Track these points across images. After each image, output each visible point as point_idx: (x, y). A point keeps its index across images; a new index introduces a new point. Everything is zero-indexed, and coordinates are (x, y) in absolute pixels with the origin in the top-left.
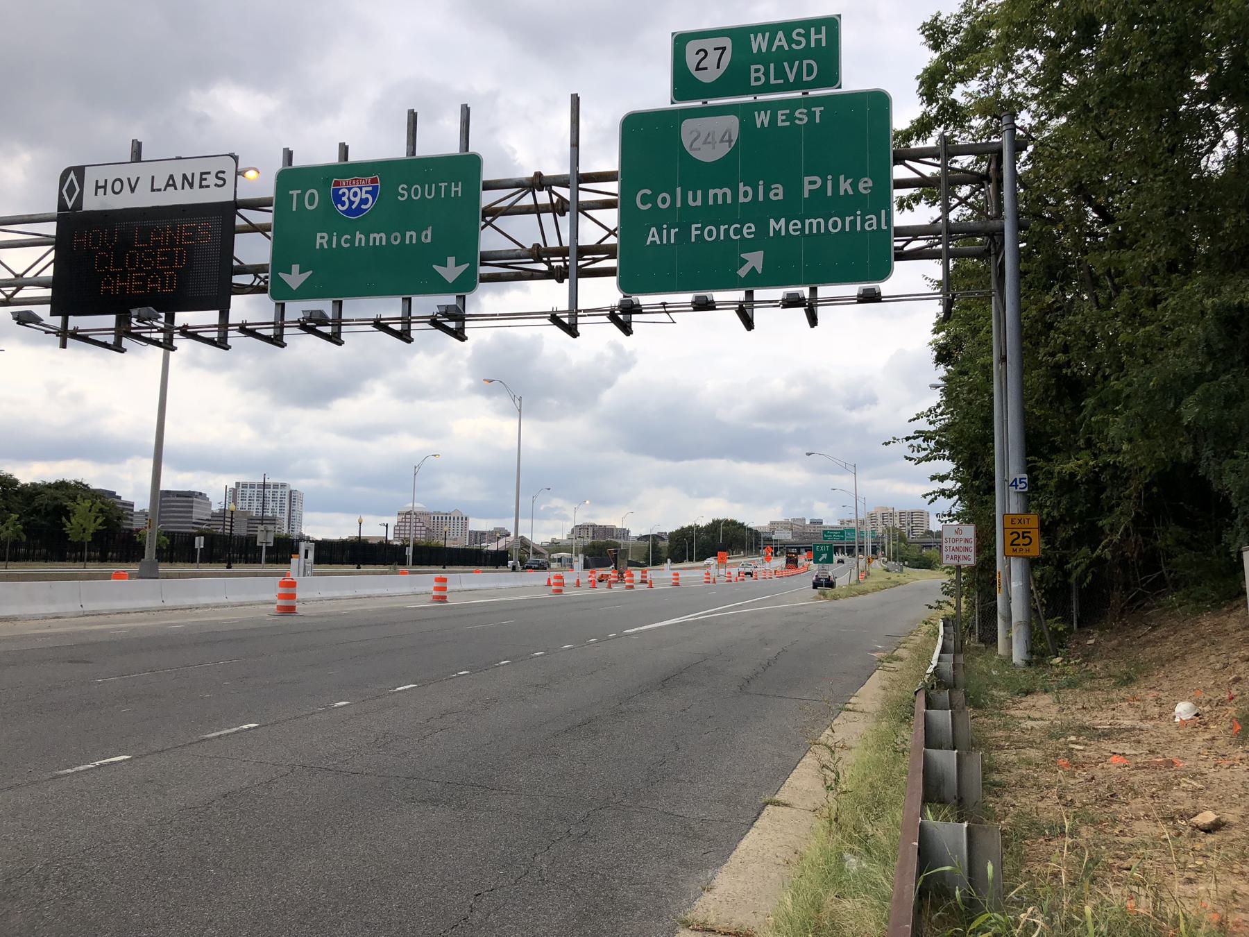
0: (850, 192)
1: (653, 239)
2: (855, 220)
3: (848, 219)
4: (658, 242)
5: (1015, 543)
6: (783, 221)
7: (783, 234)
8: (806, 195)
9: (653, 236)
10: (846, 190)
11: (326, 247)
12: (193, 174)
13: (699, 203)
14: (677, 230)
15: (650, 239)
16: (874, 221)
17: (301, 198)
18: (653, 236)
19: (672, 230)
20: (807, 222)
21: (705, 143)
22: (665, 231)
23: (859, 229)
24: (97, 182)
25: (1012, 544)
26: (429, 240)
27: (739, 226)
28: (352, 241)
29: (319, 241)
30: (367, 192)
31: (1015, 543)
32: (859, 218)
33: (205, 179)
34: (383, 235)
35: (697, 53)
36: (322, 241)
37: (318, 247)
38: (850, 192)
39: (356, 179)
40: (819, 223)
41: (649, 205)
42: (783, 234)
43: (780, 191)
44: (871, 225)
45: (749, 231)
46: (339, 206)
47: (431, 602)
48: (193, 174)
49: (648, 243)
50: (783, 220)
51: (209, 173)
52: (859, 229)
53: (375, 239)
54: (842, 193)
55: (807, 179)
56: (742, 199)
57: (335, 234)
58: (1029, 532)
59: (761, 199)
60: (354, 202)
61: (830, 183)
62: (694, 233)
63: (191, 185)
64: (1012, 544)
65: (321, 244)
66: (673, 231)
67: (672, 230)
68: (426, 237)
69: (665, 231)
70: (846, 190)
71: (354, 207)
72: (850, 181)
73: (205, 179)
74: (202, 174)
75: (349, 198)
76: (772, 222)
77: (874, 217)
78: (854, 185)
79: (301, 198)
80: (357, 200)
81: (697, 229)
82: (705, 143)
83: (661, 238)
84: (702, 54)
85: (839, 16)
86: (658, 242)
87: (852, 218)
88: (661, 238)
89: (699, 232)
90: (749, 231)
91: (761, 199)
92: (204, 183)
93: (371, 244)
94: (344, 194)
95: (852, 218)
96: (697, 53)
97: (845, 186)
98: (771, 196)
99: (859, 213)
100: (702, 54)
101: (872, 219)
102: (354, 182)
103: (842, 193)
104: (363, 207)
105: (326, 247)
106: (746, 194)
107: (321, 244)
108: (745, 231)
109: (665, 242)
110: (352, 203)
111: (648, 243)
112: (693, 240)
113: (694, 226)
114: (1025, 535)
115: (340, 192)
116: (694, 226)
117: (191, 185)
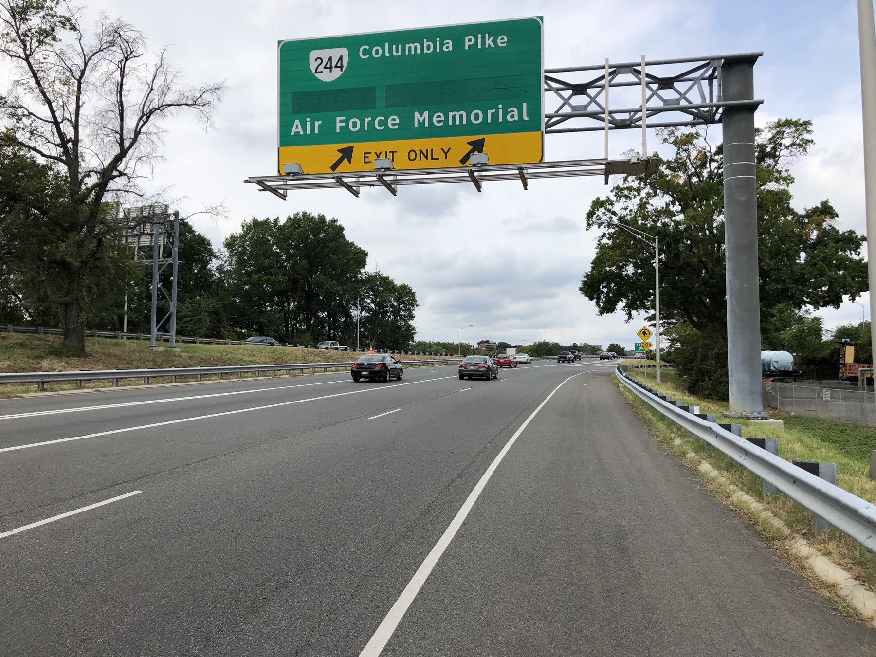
0: (493, 46)
1: (297, 130)
2: (497, 111)
3: (490, 112)
4: (302, 133)
6: (426, 114)
7: (427, 125)
8: (467, 48)
9: (297, 128)
10: (489, 44)
12: (427, 150)
13: (400, 53)
16: (516, 113)
18: (297, 128)
19: (316, 122)
20: (451, 114)
21: (325, 68)
22: (308, 123)
23: (500, 120)
24: (396, 152)
27: (383, 118)
32: (500, 111)
33: (368, 157)
35: (316, 60)
40: (461, 116)
41: (368, 56)
42: (427, 125)
43: (450, 45)
44: (513, 116)
45: (393, 122)
48: (427, 150)
49: (292, 134)
51: (370, 153)
52: (500, 120)
54: (487, 46)
56: (425, 51)
59: (438, 50)
61: (479, 39)
62: (338, 125)
63: (427, 158)
66: (317, 124)
67: (316, 122)
69: (308, 123)
70: (489, 44)
72: (492, 38)
73: (368, 157)
74: (365, 154)
76: (417, 114)
77: (515, 109)
78: (495, 41)
81: (341, 121)
82: (325, 68)
83: (304, 130)
84: (319, 61)
85: (541, 18)
86: (302, 133)
87: (494, 110)
88: (304, 130)
89: (343, 124)
90: (393, 122)
91: (438, 50)
92: (367, 160)
95: (494, 110)
96: (316, 60)
98: (445, 49)
100: (319, 61)
101: (513, 111)
103: (487, 46)
106: (428, 47)
108: (390, 122)
109: (308, 132)
112: (338, 130)
113: (338, 119)
116: (338, 119)
117: (427, 158)
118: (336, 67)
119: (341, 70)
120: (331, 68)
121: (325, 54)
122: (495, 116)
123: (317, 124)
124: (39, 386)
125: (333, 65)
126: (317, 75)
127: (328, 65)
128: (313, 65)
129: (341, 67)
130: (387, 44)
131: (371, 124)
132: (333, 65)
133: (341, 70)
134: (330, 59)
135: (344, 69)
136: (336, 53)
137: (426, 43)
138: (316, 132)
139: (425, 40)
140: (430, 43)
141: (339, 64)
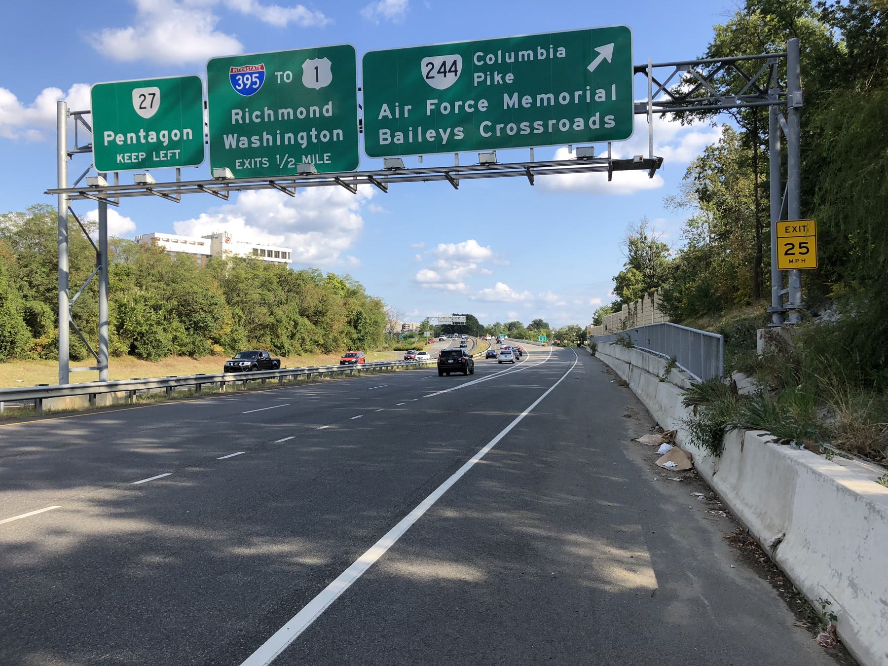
0: (501, 82)
1: (385, 114)
2: (585, 94)
4: (390, 117)
5: (789, 252)
10: (498, 81)
11: (241, 122)
13: (513, 60)
14: (410, 107)
15: (382, 114)
17: (282, 76)
18: (385, 111)
21: (439, 72)
22: (397, 109)
23: (588, 100)
25: (786, 254)
26: (330, 114)
28: (262, 116)
29: (234, 117)
30: (255, 77)
31: (789, 252)
32: (588, 93)
34: (551, 96)
35: (427, 66)
36: (237, 117)
37: (234, 122)
38: (501, 82)
39: (246, 67)
46: (237, 87)
47: (668, 321)
49: (380, 118)
50: (516, 95)
52: (588, 100)
53: (283, 114)
55: (476, 75)
57: (397, 104)
58: (807, 243)
60: (247, 84)
64: (786, 254)
65: (237, 120)
66: (407, 108)
68: (327, 111)
69: (397, 109)
70: (498, 81)
71: (247, 87)
72: (500, 75)
75: (243, 81)
76: (506, 96)
77: (603, 91)
78: (503, 78)
79: (282, 76)
80: (249, 83)
82: (439, 72)
83: (393, 113)
84: (430, 66)
86: (390, 117)
87: (581, 93)
88: (393, 113)
89: (433, 107)
91: (551, 57)
93: (280, 119)
94: (239, 79)
95: (581, 93)
96: (427, 66)
97: (498, 78)
99: (588, 88)
100: (430, 66)
102: (245, 69)
103: (496, 83)
104: (254, 86)
105: (241, 122)
107: (237, 120)
108: (480, 105)
110: (245, 85)
111: (380, 118)
114: (802, 245)
115: (237, 78)
118: (450, 71)
119: (456, 75)
120: (445, 72)
121: (438, 61)
122: (582, 98)
123: (407, 108)
124: (35, 403)
125: (447, 70)
126: (428, 81)
127: (442, 70)
128: (424, 70)
129: (456, 71)
130: (500, 52)
131: (461, 108)
132: (447, 70)
133: (456, 75)
134: (444, 64)
135: (459, 73)
136: (449, 59)
137: (540, 50)
138: (406, 115)
139: (539, 48)
140: (543, 51)
141: (453, 69)
